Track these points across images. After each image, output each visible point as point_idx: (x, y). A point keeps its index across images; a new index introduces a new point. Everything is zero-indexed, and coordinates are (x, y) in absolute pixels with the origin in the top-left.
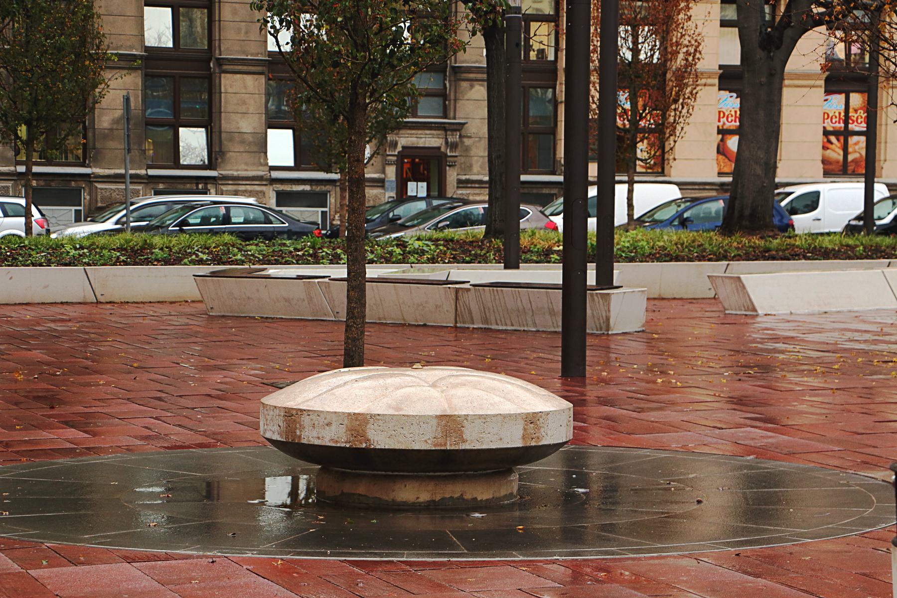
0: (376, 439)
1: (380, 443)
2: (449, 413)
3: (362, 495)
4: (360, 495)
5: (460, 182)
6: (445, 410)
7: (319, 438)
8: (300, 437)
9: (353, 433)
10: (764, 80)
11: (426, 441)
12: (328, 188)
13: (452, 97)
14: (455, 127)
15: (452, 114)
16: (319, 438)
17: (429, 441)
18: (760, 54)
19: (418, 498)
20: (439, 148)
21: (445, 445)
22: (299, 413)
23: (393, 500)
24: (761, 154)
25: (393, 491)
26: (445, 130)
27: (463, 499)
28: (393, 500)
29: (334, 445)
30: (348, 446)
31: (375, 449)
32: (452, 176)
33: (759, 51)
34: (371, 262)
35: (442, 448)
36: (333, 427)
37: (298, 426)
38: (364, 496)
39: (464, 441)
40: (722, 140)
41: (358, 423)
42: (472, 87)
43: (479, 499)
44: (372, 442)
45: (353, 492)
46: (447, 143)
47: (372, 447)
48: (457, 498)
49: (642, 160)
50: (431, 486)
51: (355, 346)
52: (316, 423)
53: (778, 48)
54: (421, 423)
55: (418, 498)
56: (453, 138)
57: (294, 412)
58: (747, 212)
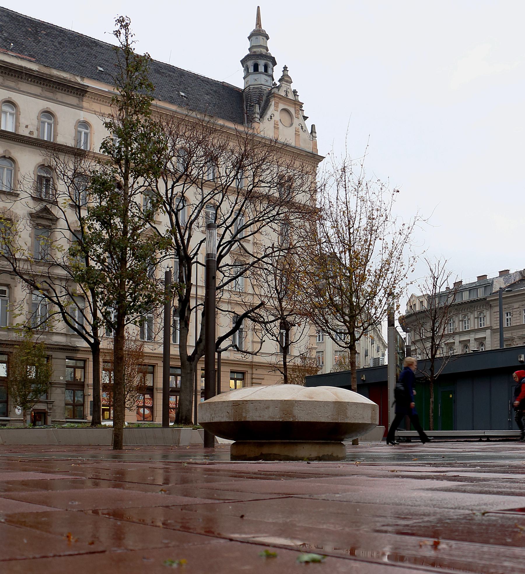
0: (299, 415)
1: (301, 418)
2: (339, 400)
3: (276, 455)
4: (274, 454)
5: (52, 421)
6: (336, 399)
7: (260, 417)
8: (245, 417)
9: (284, 412)
10: (189, 371)
11: (328, 417)
12: (7, 423)
13: (50, 393)
14: (50, 402)
15: (49, 398)
16: (260, 417)
17: (329, 417)
18: (187, 363)
19: (310, 455)
20: (45, 410)
21: (338, 419)
22: (245, 403)
23: (296, 456)
24: (188, 398)
25: (297, 451)
26: (47, 403)
27: (333, 456)
28: (296, 456)
29: (271, 420)
30: (281, 420)
31: (298, 422)
32: (49, 419)
33: (187, 361)
34: (144, 383)
35: (337, 421)
36: (271, 409)
37: (244, 410)
38: (278, 454)
39: (347, 418)
40: (138, 409)
41: (287, 406)
42: (56, 389)
43: (339, 456)
44: (297, 418)
45: (270, 453)
46: (48, 408)
47: (297, 420)
48: (330, 456)
49: (127, 408)
50: (317, 447)
51: (120, 432)
52: (258, 407)
53: (193, 361)
54: (325, 406)
55: (310, 455)
56: (50, 406)
57: (241, 403)
58: (184, 418)
